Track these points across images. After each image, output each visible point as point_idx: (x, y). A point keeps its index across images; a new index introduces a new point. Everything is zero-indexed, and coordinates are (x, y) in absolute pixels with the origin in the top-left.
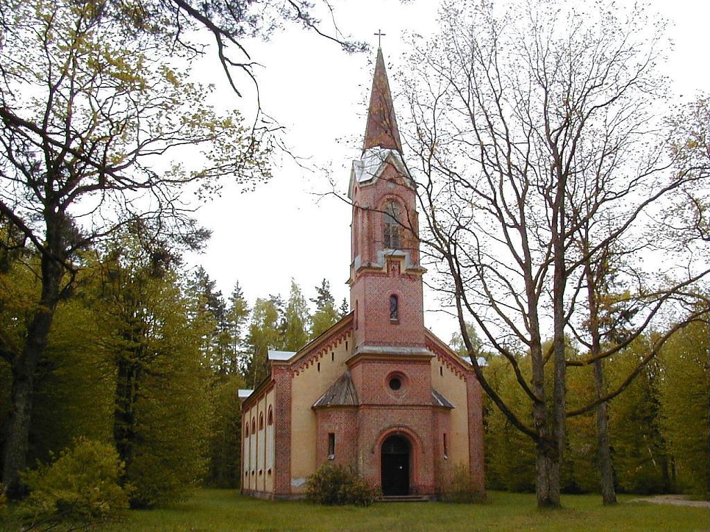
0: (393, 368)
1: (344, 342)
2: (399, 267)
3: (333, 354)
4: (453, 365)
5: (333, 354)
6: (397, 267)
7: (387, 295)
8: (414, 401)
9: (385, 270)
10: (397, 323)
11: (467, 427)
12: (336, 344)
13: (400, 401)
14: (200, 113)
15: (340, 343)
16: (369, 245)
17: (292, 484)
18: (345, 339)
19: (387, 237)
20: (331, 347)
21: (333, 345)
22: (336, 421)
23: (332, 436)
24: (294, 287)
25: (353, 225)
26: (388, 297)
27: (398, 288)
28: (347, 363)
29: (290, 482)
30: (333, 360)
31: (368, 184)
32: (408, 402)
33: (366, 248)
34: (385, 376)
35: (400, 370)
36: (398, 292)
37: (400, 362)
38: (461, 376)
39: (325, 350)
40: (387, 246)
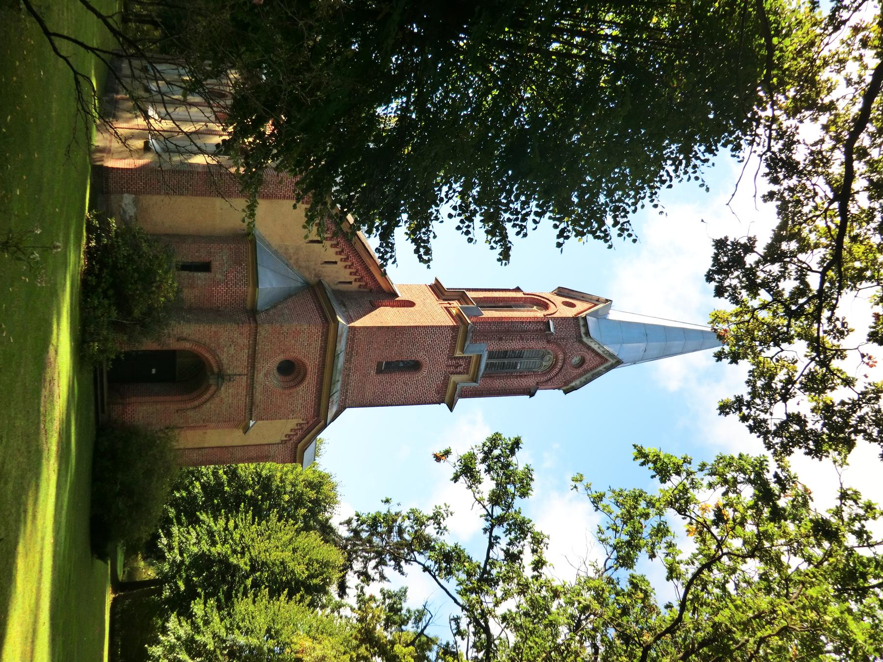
0: (311, 364)
1: (337, 258)
2: (460, 373)
3: (336, 263)
4: (306, 427)
5: (336, 263)
6: (460, 369)
7: (421, 356)
8: (258, 396)
9: (458, 354)
10: (379, 371)
11: (216, 445)
12: (350, 267)
13: (260, 377)
14: (833, 128)
15: (346, 267)
16: (498, 331)
17: (125, 195)
18: (341, 260)
19: (504, 354)
20: (346, 260)
21: (349, 263)
22: (231, 276)
23: (206, 267)
24: (635, 446)
25: (520, 295)
26: (418, 359)
27: (430, 372)
28: (320, 284)
29: (128, 192)
30: (326, 262)
31: (583, 330)
32: (259, 388)
33: (494, 328)
34: (300, 357)
35: (309, 372)
36: (424, 372)
37: (320, 383)
38: (289, 436)
39: (342, 251)
40: (491, 355)
